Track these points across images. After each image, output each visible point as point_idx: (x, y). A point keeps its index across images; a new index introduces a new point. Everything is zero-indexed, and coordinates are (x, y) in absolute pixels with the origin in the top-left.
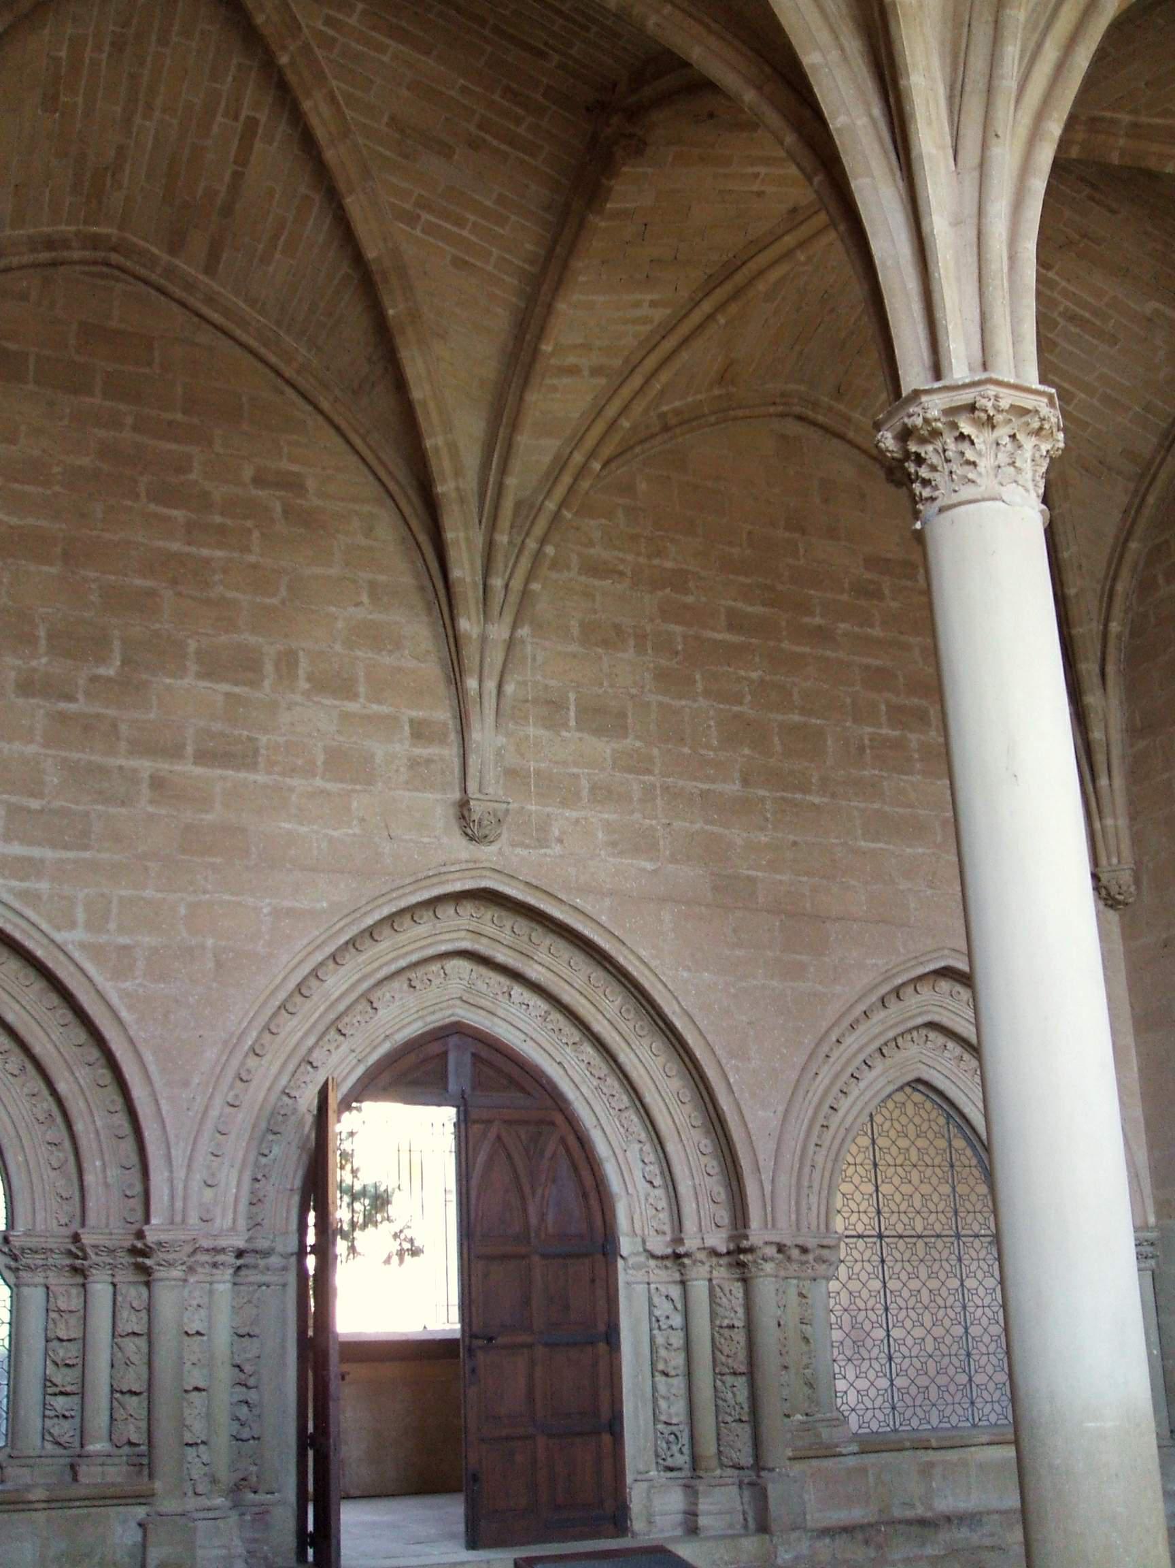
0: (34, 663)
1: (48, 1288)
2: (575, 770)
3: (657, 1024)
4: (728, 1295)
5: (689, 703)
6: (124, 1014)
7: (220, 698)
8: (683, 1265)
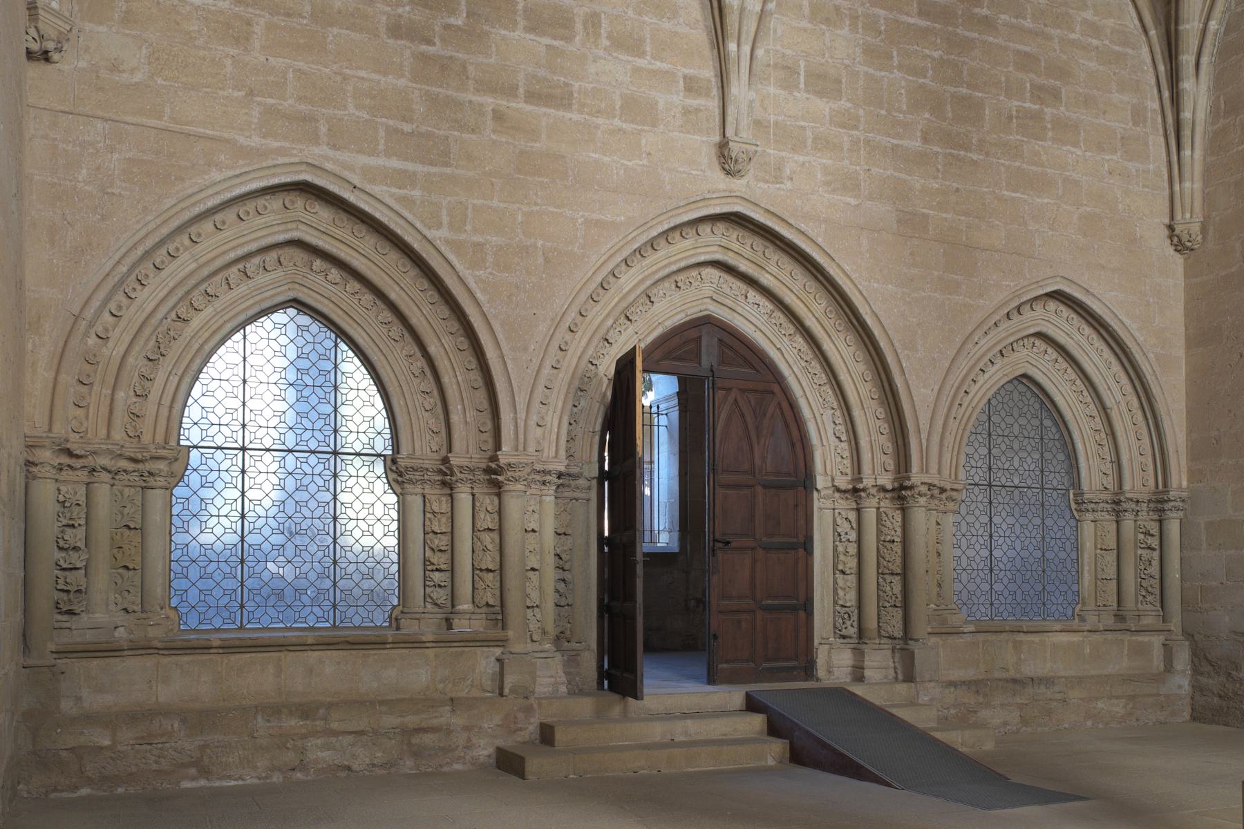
0: (400, 10)
1: (424, 497)
2: (802, 124)
3: (851, 323)
4: (891, 518)
5: (887, 73)
6: (479, 295)
7: (543, 49)
8: (860, 497)
